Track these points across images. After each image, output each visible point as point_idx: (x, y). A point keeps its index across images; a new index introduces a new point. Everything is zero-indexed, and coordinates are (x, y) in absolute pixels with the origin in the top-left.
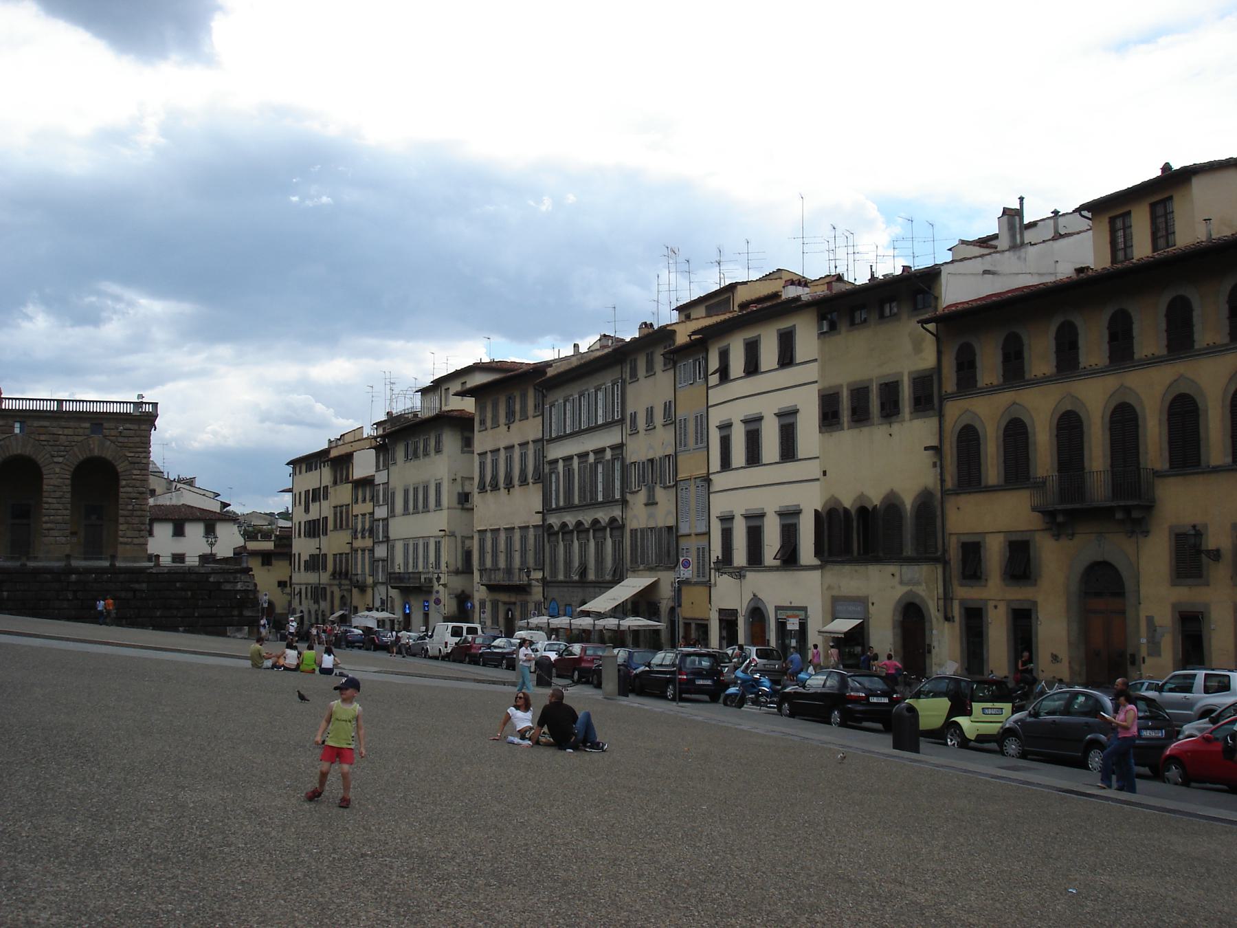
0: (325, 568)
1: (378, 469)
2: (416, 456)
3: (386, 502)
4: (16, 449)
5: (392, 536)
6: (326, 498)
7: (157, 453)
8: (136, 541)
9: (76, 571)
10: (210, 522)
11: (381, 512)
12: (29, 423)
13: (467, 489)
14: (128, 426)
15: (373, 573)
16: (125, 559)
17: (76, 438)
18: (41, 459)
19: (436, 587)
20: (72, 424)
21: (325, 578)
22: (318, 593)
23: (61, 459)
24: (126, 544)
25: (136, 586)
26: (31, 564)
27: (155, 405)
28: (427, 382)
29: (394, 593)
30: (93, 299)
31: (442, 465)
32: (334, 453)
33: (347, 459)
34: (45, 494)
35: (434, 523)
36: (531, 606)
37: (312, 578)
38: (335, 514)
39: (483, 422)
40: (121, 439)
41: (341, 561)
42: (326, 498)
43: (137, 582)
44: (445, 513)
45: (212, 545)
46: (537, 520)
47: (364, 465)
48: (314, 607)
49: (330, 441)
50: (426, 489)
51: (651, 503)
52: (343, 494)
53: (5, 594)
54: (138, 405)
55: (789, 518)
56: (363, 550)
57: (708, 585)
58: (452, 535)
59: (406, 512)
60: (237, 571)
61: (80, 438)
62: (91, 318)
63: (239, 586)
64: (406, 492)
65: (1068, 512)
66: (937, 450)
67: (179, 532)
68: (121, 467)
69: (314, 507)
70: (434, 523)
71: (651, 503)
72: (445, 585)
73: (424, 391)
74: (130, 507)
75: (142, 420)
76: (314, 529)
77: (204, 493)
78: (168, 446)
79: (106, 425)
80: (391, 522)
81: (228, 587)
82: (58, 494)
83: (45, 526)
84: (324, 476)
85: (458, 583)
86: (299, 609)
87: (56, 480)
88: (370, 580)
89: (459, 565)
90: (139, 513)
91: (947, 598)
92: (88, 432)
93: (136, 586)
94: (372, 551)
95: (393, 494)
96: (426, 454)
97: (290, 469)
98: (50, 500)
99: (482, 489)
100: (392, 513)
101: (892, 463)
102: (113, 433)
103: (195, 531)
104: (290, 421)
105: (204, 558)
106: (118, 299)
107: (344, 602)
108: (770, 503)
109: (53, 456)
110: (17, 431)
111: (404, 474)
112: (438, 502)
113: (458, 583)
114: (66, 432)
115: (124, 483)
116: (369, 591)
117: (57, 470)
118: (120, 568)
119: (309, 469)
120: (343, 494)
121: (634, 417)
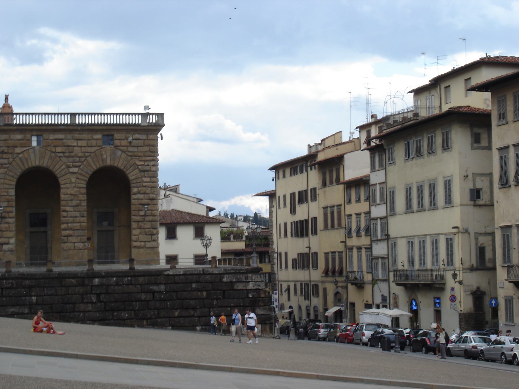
0: (315, 266)
1: (373, 168)
2: (419, 153)
3: (383, 201)
4: (35, 162)
5: (393, 233)
8: (149, 245)
9: (98, 275)
10: (199, 225)
11: (379, 211)
12: (45, 136)
13: (478, 186)
14: (137, 136)
15: (372, 269)
16: (141, 263)
17: (89, 149)
18: (58, 170)
19: (450, 282)
20: (85, 136)
21: (316, 275)
22: (309, 290)
23: (76, 170)
24: (139, 247)
25: (155, 288)
26: (56, 270)
27: (161, 116)
29: (399, 291)
30: (35, 41)
31: (453, 161)
32: (321, 157)
33: (337, 162)
34: (62, 203)
35: (446, 220)
37: (302, 275)
38: (325, 215)
39: (502, 116)
40: (131, 149)
41: (334, 260)
42: (314, 198)
43: (156, 284)
45: (206, 246)
47: (357, 165)
48: (304, 303)
49: (310, 147)
50: (433, 187)
52: (334, 195)
53: (34, 298)
54: (145, 116)
56: (359, 249)
58: (466, 231)
60: (248, 272)
61: (93, 149)
62: (34, 57)
63: (251, 286)
64: (408, 191)
67: (171, 235)
68: (132, 175)
70: (446, 220)
72: (460, 282)
73: (418, 92)
74: (142, 213)
75: (148, 130)
76: (302, 229)
77: (186, 198)
78: (170, 150)
79: (117, 136)
80: (391, 221)
81: (240, 286)
82: (75, 203)
83: (64, 233)
84: (312, 178)
85: (474, 280)
86: (287, 304)
87: (73, 189)
88: (368, 278)
89: (474, 262)
90: (151, 218)
92: (100, 143)
93: (155, 288)
94: (369, 249)
95: (392, 194)
96: (431, 151)
97: (273, 174)
98: (68, 208)
99: (504, 184)
100: (392, 211)
102: (124, 143)
103: (185, 233)
104: (205, 138)
105: (199, 259)
106: (55, 41)
107: (338, 298)
109: (68, 167)
110: (34, 144)
111: (404, 172)
112: (448, 200)
113: (474, 280)
114: (80, 143)
115: (135, 190)
116: (368, 288)
117: (73, 180)
118: (140, 271)
119: (294, 172)
120: (334, 195)
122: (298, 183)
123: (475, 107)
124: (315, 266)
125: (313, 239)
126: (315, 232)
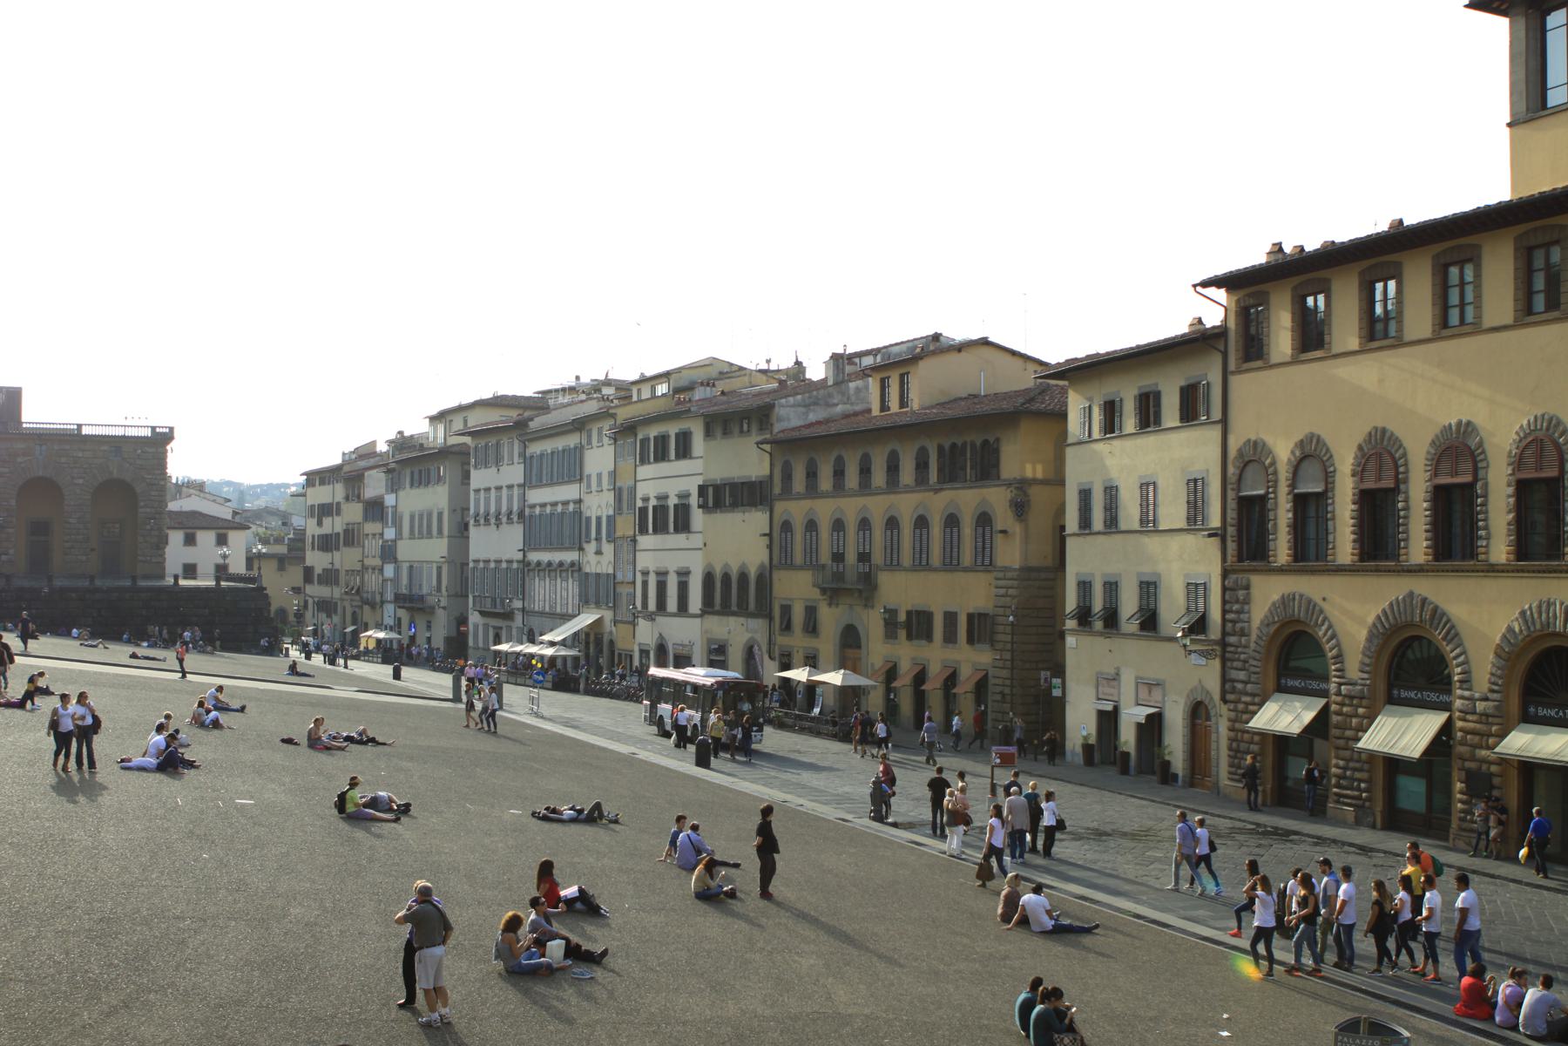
6: (338, 514)
7: (170, 471)
10: (222, 530)
11: (390, 533)
21: (337, 592)
28: (434, 412)
29: (402, 613)
36: (514, 632)
42: (338, 514)
44: (446, 540)
46: (520, 556)
51: (599, 552)
55: (684, 574)
57: (634, 624)
59: (412, 536)
64: (412, 518)
65: (834, 591)
66: (770, 535)
67: (190, 540)
69: (327, 521)
71: (599, 552)
76: (327, 543)
78: (179, 466)
91: (770, 643)
101: (739, 540)
103: (206, 538)
108: (673, 563)
121: (589, 476)
122: (322, 495)
123: (254, 482)
124: (337, 583)
125: (337, 555)
126: (338, 549)
